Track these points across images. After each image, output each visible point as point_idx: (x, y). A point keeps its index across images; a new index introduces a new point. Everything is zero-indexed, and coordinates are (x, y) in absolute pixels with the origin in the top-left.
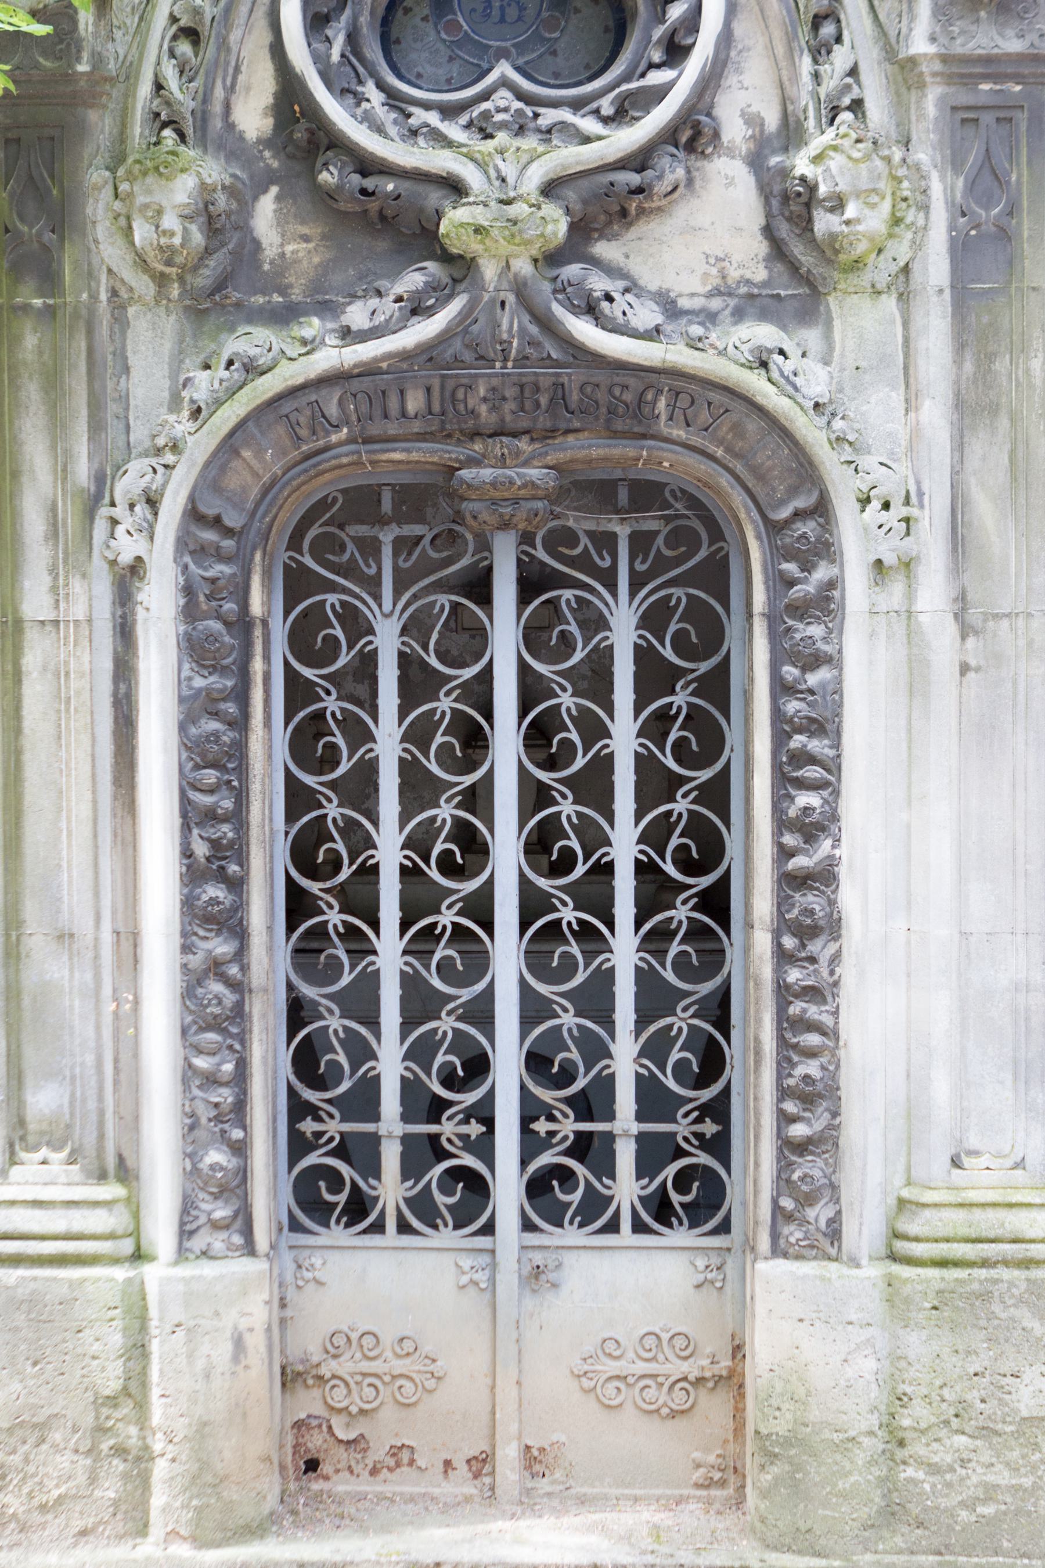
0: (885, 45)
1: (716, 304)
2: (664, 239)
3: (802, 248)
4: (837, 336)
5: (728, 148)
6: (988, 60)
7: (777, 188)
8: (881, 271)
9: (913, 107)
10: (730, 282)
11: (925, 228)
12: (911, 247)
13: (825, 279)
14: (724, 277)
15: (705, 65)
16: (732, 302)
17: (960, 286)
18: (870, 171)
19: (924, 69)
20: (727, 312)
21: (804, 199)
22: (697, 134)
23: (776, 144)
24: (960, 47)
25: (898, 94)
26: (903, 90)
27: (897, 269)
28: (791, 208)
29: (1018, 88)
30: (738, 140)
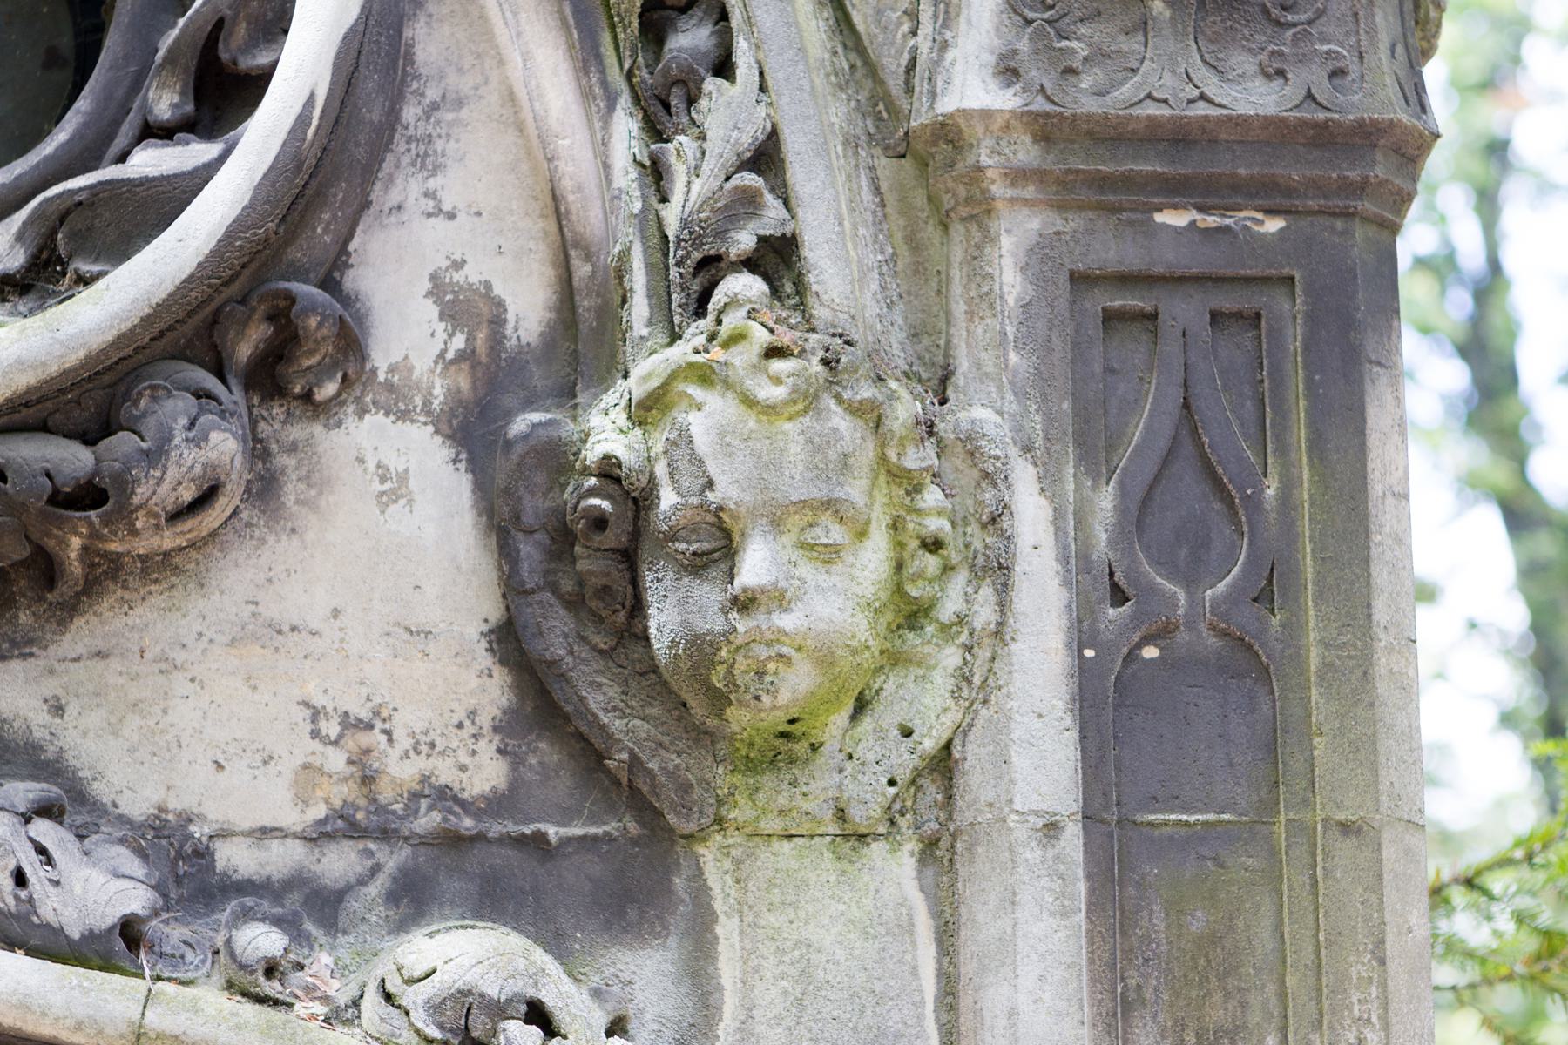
0: (874, 100)
1: (338, 863)
2: (180, 656)
3: (613, 691)
4: (728, 969)
5: (389, 387)
6: (1178, 137)
7: (534, 506)
8: (863, 765)
9: (957, 274)
10: (386, 793)
11: (999, 633)
12: (955, 694)
13: (686, 788)
14: (367, 780)
15: (302, 120)
16: (392, 859)
17: (1112, 816)
18: (815, 446)
19: (985, 160)
20: (374, 890)
21: (613, 537)
22: (285, 342)
23: (538, 378)
24: (1087, 98)
25: (914, 243)
26: (931, 231)
27: (913, 761)
28: (581, 565)
29: (1273, 225)
30: (422, 364)
